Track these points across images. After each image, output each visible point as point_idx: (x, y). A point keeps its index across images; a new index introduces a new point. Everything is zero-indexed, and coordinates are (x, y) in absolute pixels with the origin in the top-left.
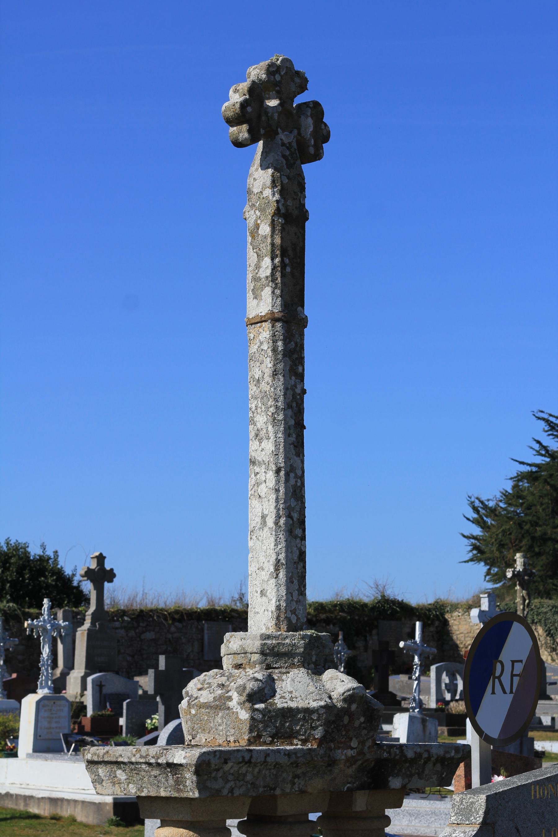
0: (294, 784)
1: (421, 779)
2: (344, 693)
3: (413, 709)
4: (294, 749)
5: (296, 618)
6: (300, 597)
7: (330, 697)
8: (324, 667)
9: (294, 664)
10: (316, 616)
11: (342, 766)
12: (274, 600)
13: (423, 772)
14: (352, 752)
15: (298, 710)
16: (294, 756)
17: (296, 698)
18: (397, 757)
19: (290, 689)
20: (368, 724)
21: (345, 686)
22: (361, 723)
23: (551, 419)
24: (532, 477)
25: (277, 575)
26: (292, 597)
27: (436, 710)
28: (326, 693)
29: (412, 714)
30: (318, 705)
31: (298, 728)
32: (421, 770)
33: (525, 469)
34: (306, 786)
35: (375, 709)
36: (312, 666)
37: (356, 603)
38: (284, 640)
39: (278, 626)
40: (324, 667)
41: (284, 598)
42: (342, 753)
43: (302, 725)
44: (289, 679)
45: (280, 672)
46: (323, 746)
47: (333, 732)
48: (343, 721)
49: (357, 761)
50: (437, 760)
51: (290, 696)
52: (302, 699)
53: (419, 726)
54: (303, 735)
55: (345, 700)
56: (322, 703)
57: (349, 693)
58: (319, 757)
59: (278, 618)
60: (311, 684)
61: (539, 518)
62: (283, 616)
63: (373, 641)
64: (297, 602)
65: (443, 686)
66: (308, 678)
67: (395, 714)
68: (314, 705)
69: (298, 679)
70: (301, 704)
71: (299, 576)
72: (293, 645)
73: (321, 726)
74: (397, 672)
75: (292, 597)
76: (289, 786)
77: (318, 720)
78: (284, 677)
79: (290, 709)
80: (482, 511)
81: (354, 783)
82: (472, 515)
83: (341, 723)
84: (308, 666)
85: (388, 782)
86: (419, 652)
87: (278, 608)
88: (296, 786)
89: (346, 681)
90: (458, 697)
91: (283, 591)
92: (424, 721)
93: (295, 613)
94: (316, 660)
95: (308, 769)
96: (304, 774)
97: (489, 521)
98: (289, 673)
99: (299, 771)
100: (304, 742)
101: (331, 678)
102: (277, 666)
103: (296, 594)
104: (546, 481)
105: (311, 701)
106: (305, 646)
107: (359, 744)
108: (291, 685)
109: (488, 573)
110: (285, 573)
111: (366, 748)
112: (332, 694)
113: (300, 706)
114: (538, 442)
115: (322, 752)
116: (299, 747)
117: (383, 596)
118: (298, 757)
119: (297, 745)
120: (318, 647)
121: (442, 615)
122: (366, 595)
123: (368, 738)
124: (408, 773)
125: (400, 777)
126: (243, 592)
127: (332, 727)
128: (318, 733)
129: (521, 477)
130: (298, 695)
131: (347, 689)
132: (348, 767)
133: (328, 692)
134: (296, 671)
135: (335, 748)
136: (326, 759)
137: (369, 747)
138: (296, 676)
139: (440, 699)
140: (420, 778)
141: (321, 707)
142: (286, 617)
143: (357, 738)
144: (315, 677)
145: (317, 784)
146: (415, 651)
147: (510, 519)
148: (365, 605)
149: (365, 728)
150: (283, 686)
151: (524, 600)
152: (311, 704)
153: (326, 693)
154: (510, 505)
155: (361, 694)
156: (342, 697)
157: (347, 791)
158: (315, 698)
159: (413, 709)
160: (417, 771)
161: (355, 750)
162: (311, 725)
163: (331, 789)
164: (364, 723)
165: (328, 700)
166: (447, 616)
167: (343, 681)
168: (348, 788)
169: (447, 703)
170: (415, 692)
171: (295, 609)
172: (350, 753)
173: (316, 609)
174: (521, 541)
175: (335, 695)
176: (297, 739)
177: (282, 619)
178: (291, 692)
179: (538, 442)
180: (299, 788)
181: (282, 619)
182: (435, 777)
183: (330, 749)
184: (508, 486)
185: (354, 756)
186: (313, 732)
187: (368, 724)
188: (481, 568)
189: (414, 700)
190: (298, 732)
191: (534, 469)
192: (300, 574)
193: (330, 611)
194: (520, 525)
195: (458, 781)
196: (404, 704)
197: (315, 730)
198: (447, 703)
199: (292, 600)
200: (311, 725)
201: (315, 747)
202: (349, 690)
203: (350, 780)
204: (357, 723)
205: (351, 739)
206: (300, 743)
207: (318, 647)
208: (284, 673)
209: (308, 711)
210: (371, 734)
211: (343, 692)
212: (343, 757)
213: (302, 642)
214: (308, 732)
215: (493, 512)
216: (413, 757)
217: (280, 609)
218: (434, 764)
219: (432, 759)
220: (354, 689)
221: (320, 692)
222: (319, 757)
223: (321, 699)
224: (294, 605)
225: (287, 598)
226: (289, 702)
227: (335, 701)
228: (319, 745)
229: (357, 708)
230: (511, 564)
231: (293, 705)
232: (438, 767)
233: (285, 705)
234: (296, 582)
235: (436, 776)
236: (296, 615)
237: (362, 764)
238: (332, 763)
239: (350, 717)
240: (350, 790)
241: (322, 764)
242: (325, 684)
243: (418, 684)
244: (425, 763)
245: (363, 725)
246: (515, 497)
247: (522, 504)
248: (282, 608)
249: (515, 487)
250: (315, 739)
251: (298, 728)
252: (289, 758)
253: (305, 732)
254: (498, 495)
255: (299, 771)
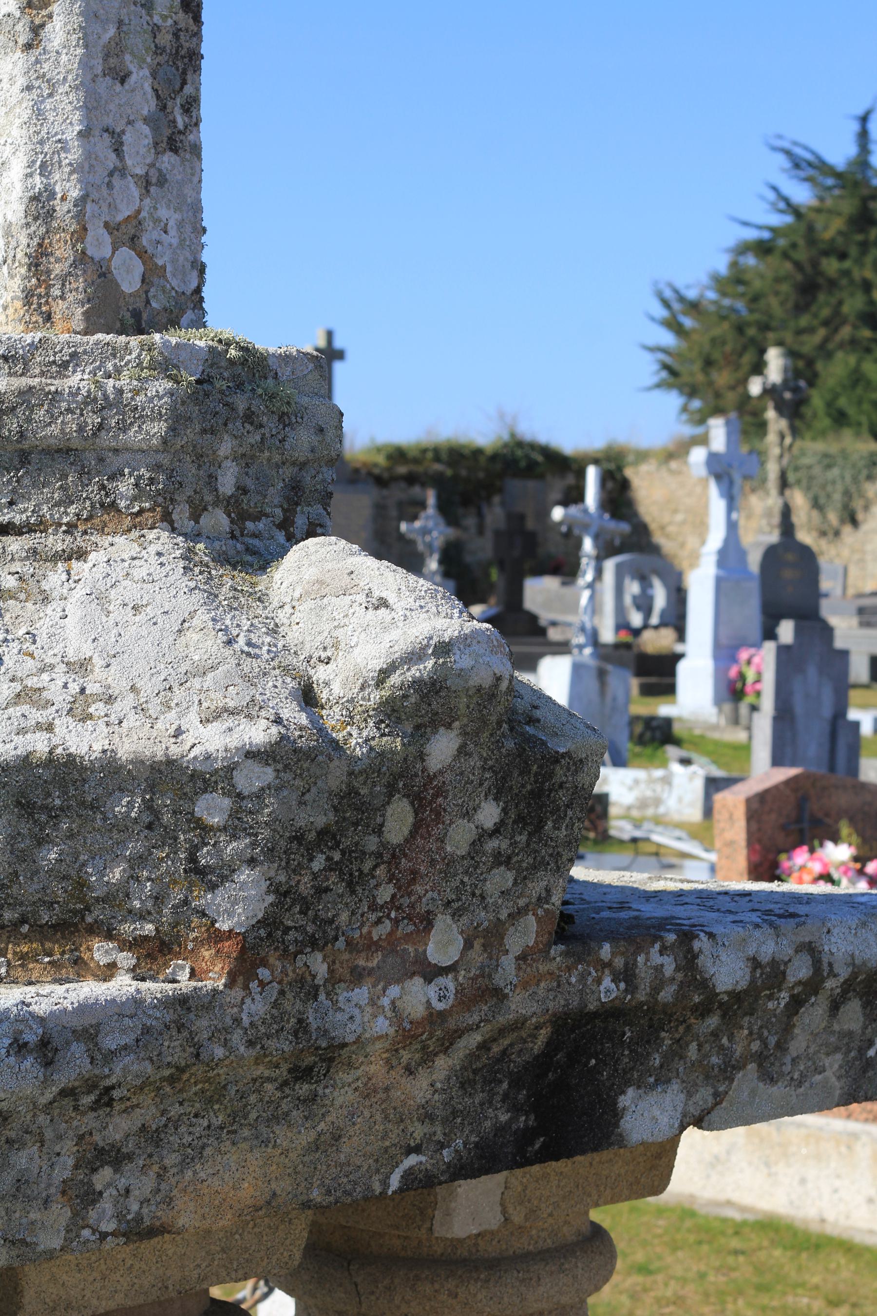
0: (91, 1197)
1: (772, 1081)
2: (384, 674)
3: (581, 647)
4: (83, 1008)
5: (138, 268)
6: (168, 160)
7: (308, 697)
8: (285, 525)
9: (113, 505)
10: (389, 469)
11: (376, 1068)
12: (17, 168)
13: (781, 1046)
14: (432, 992)
15: (112, 772)
16: (78, 1049)
17: (110, 700)
18: (667, 995)
19: (77, 646)
20: (522, 838)
21: (395, 634)
22: (484, 835)
23: (798, 151)
24: (762, 248)
25: (36, 30)
26: (118, 151)
27: (617, 646)
28: (286, 670)
29: (578, 658)
30: (234, 741)
31: (116, 874)
32: (772, 1041)
33: (751, 234)
34: (169, 1201)
35: (556, 758)
36: (218, 520)
37: (463, 447)
38: (61, 375)
39: (36, 302)
40: (285, 525)
41: (74, 155)
42: (373, 1002)
43: (139, 861)
44: (80, 591)
45: (34, 553)
46: (264, 973)
47: (321, 891)
48: (379, 830)
49: (459, 1033)
50: (848, 986)
51: (74, 688)
52: (140, 709)
53: (592, 684)
54: (143, 916)
55: (390, 713)
56: (258, 733)
57: (415, 672)
58: (237, 1038)
59: (37, 261)
60: (203, 617)
61: (771, 317)
62: (63, 251)
63: (495, 515)
64: (146, 184)
65: (628, 600)
66: (185, 583)
67: (542, 655)
68: (210, 741)
69: (129, 591)
70: (134, 740)
71: (159, 50)
72: (108, 405)
73: (252, 862)
74: (540, 571)
75: (118, 151)
76: (60, 1214)
77: (232, 830)
78: (55, 578)
79: (65, 770)
80: (677, 306)
81: (442, 1146)
82: (661, 312)
83: (372, 843)
84: (196, 517)
85: (616, 1115)
86: (594, 529)
87: (40, 206)
88: (106, 1205)
89: (400, 603)
90: (655, 620)
91: (67, 118)
92: (602, 674)
93: (133, 241)
94: (242, 490)
95: (175, 1110)
96: (152, 1137)
97: (688, 322)
98: (81, 555)
99: (119, 1128)
100: (153, 953)
101: (319, 590)
102: (18, 519)
103: (139, 142)
104: (785, 255)
105: (191, 720)
106: (173, 409)
107: (468, 945)
108: (86, 622)
109: (685, 409)
110: (77, 20)
111: (508, 963)
112: (320, 674)
113: (125, 750)
114: (775, 189)
115: (257, 1007)
116: (123, 985)
117: (513, 435)
118: (111, 1056)
119: (109, 971)
120: (249, 417)
121: (620, 469)
122: (482, 432)
123: (521, 912)
124: (715, 1060)
125: (675, 1086)
126: (685, 745)
127: (319, 863)
128: (239, 903)
129: (744, 248)
130: (119, 685)
131: (402, 647)
132: (410, 1071)
133: (297, 662)
134: (123, 545)
135: (333, 979)
136: (283, 1045)
137: (522, 958)
138: (118, 571)
139: (622, 625)
140: (769, 1078)
141: (252, 754)
142: (82, 259)
143: (457, 915)
144: (228, 580)
145: (237, 1177)
146: (586, 528)
147: (723, 318)
148: (478, 452)
149: (501, 860)
150: (43, 630)
151: (782, 437)
152: (188, 739)
153: (286, 670)
154: (724, 294)
155: (483, 678)
156: (375, 696)
157: (400, 1190)
158: (217, 700)
159: (581, 647)
160: (755, 1046)
161: (448, 982)
162: (192, 859)
163: (316, 1195)
164: (496, 831)
165: (294, 715)
166: (629, 472)
167: (383, 603)
168: (408, 1174)
169: (637, 632)
170: (585, 612)
171: (135, 219)
172: (418, 997)
173: (390, 457)
174: (740, 355)
175: (336, 682)
176: (109, 936)
177: (58, 269)
178: (82, 666)
179: (775, 189)
180: (119, 1216)
181: (58, 269)
182: (833, 1063)
183: (308, 989)
184: (721, 264)
185: (442, 1014)
186: (205, 900)
187: (522, 838)
188: (673, 400)
189: (583, 629)
190: (115, 898)
191: (766, 235)
192: (165, 39)
193: (416, 461)
194: (740, 329)
195: (727, 858)
196: (554, 635)
197: (212, 887)
198: (637, 632)
199: (121, 171)
200: (192, 859)
201: (215, 980)
202: (414, 657)
203: (419, 1131)
204: (459, 837)
205: (427, 922)
206: (126, 959)
207: (249, 417)
208: (56, 558)
209: (172, 781)
210: (536, 888)
211: (379, 664)
212: (382, 1025)
213: (162, 385)
214: (177, 896)
215: (694, 307)
216: (743, 985)
217: (51, 213)
218: (835, 1007)
219: (830, 984)
220: (443, 649)
221: (248, 664)
222: (237, 1038)
223: (249, 711)
224: (128, 199)
225: (88, 155)
226: (62, 725)
227: (332, 717)
228: (243, 970)
229: (462, 751)
230: (759, 368)
231: (84, 741)
232: (853, 1015)
233: (39, 744)
234: (141, 77)
235: (839, 1056)
236: (142, 254)
237: (484, 1046)
238: (314, 1062)
239: (418, 802)
240: (420, 1183)
241: (261, 1070)
242: (282, 617)
243: (592, 598)
244: (796, 1003)
245: (492, 845)
246: (734, 281)
247: (743, 295)
248: (61, 209)
249: (734, 265)
250: (216, 937)
251: (116, 874)
252: (48, 1064)
253: (158, 899)
254: (705, 279)
255: (119, 1128)
